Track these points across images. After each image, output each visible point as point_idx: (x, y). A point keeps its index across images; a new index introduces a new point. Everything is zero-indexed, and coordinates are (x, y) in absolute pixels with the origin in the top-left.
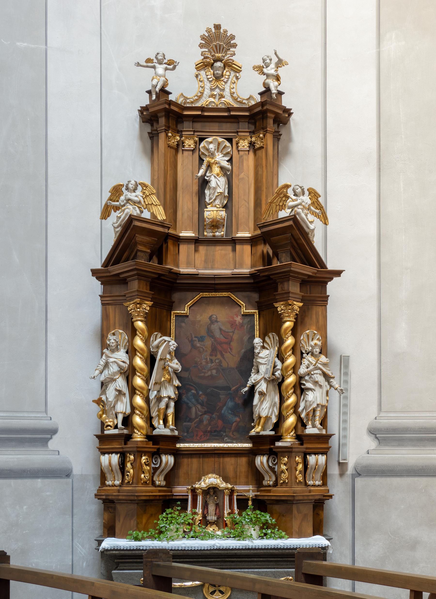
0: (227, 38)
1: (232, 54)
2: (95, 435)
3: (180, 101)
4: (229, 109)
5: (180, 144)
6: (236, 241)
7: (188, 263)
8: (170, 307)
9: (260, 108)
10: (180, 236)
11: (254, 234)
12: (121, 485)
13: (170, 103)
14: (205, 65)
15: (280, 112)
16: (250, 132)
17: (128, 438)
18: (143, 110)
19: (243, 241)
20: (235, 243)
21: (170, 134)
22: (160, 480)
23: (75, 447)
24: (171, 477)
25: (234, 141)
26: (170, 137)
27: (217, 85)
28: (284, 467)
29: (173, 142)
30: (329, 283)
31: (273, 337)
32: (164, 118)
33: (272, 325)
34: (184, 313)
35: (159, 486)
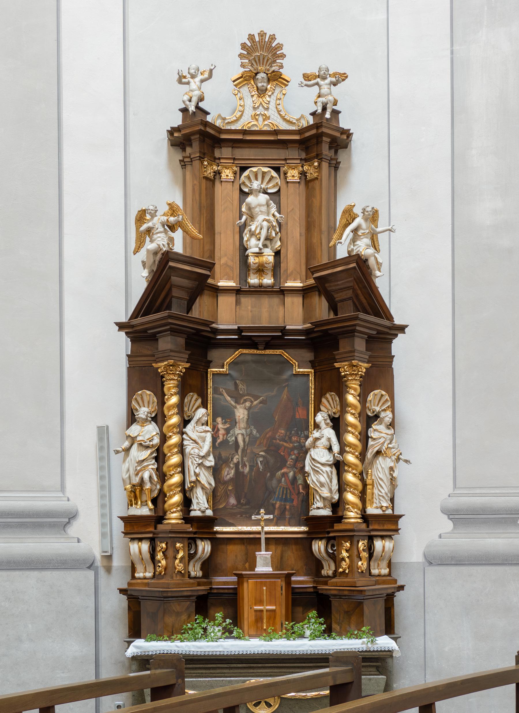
0: (271, 48)
1: (280, 66)
2: (118, 517)
3: (218, 123)
4: (276, 132)
5: (218, 173)
6: (285, 292)
7: (227, 315)
8: (208, 364)
9: (314, 132)
10: (219, 286)
11: (306, 284)
12: (154, 576)
13: (206, 124)
14: (247, 78)
15: (338, 134)
16: (301, 159)
17: (159, 518)
18: (171, 132)
19: (293, 291)
20: (284, 294)
21: (206, 163)
22: (195, 571)
23: (95, 528)
24: (209, 567)
25: (282, 170)
26: (207, 166)
27: (261, 103)
28: (345, 554)
29: (209, 172)
30: (394, 341)
31: (332, 399)
32: (198, 140)
33: (331, 383)
34: (223, 371)
35: (195, 578)
